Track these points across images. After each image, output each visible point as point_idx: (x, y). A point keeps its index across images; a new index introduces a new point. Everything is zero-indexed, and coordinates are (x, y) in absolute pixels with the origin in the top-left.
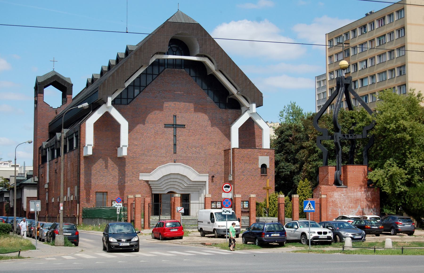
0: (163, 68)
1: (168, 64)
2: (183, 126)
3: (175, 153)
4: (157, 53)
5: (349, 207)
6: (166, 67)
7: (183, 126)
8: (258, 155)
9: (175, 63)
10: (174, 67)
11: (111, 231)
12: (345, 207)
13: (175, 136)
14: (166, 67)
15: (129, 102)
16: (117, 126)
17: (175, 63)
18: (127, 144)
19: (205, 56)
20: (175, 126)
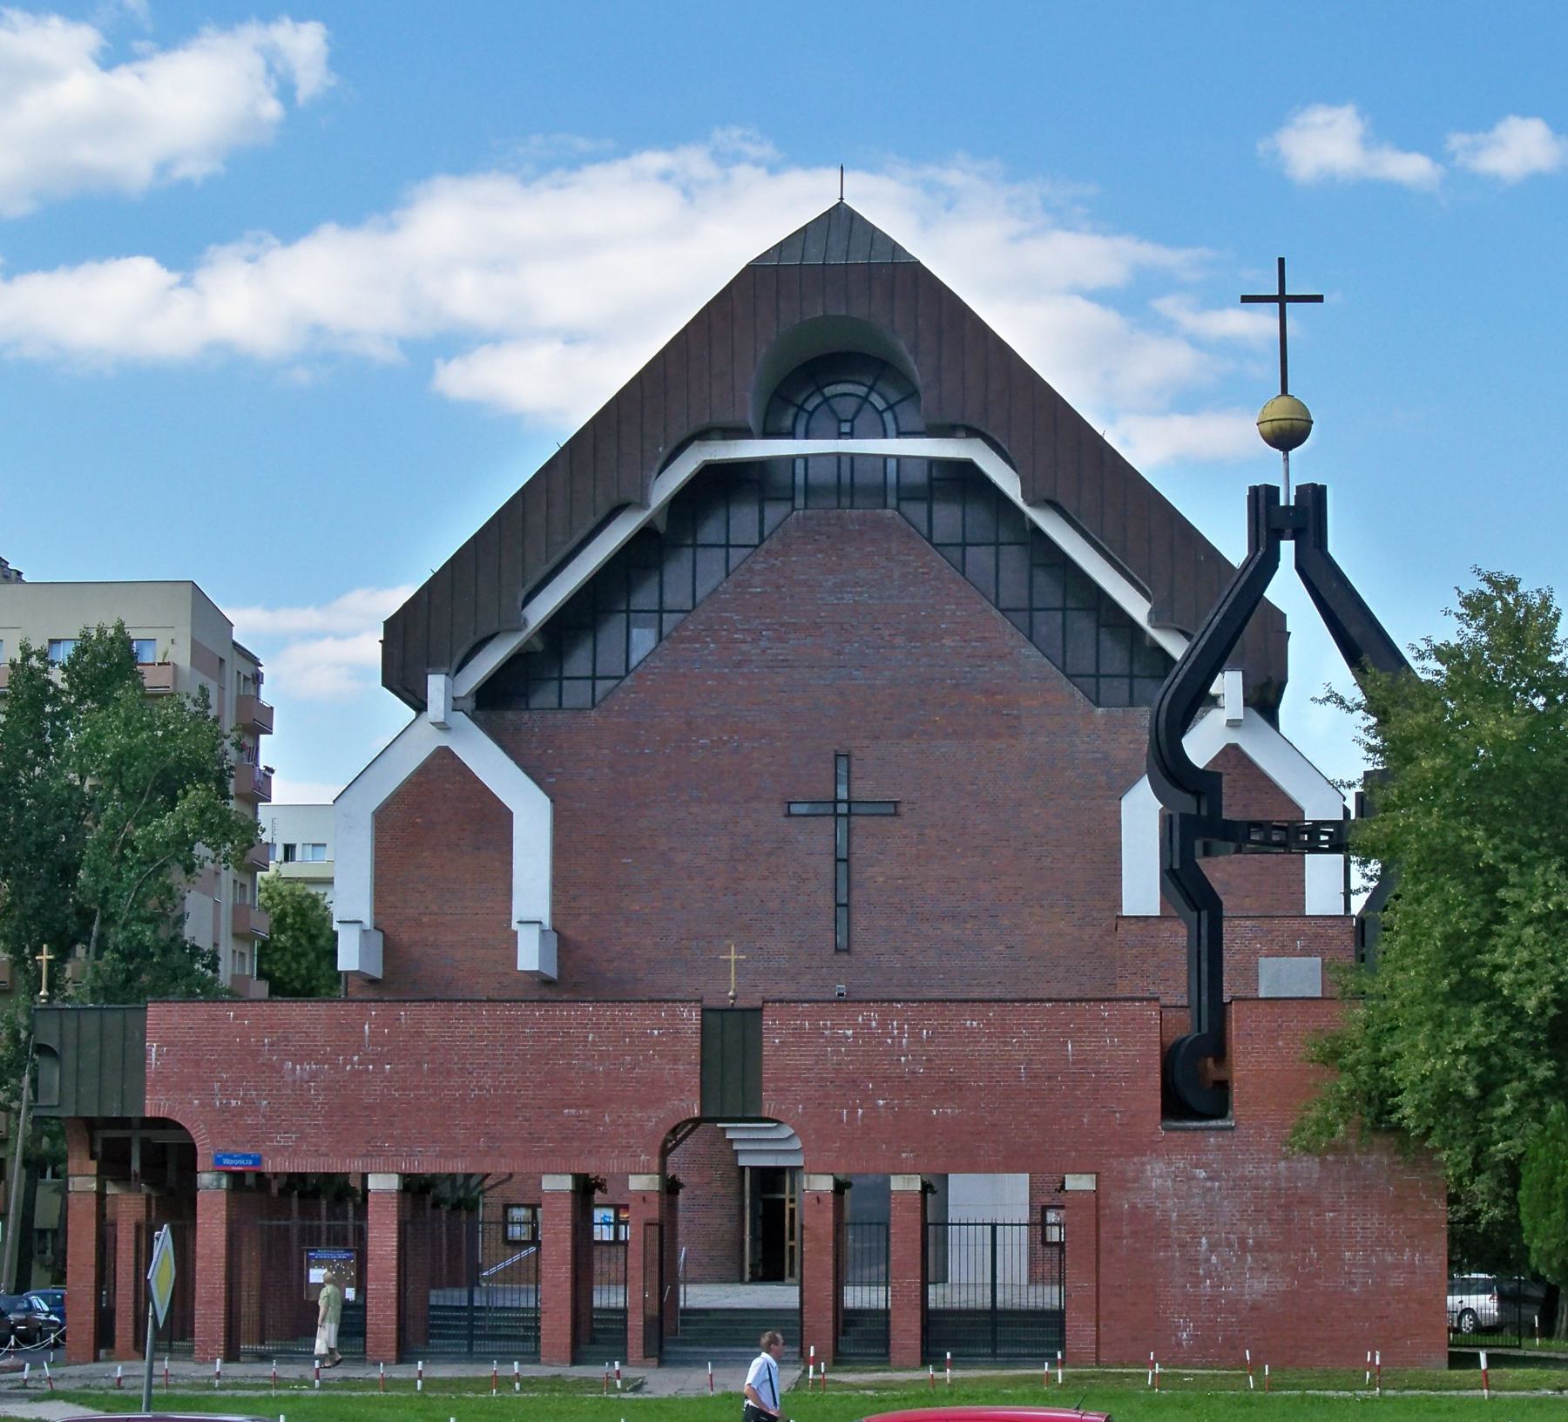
0: (784, 508)
1: (809, 490)
2: (893, 809)
3: (843, 950)
4: (704, 435)
5: (1242, 1242)
6: (800, 502)
7: (893, 809)
8: (1256, 953)
9: (846, 478)
10: (846, 501)
11: (155, 1372)
12: (1213, 1247)
13: (843, 861)
14: (800, 502)
15: (599, 696)
16: (494, 822)
17: (846, 478)
18: (365, 913)
19: (972, 432)
20: (841, 811)
